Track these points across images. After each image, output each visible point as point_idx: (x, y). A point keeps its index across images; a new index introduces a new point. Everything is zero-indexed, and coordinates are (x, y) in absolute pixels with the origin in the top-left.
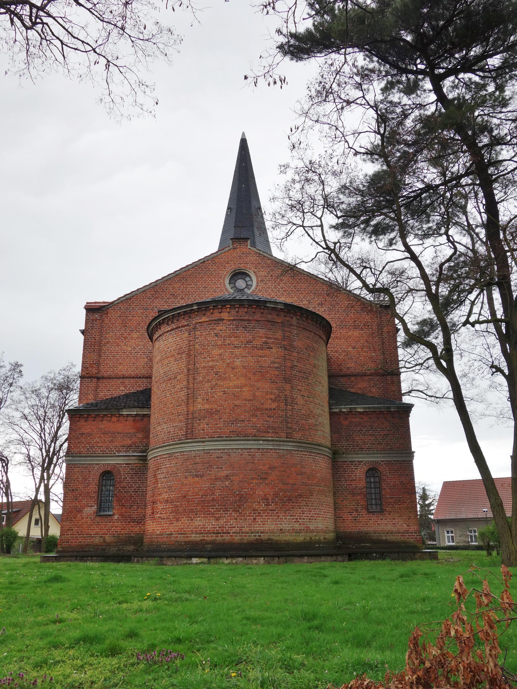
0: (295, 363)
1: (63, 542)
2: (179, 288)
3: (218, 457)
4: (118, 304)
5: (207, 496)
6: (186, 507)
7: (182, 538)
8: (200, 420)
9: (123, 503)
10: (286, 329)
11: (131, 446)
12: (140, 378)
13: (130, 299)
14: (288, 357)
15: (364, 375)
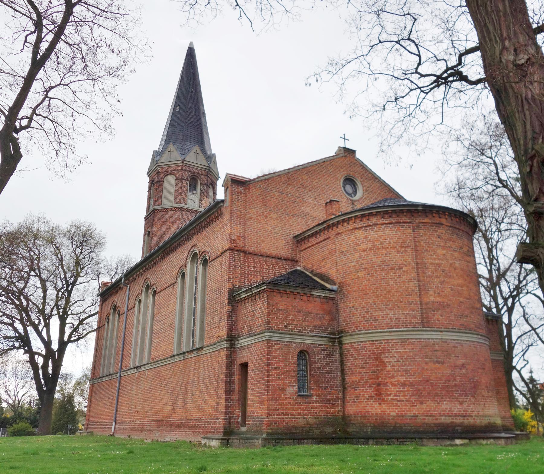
1: (271, 424)
2: (307, 180)
3: (454, 347)
4: (258, 181)
5: (449, 381)
6: (431, 391)
7: (430, 420)
8: (434, 311)
9: (319, 384)
11: (320, 327)
12: (281, 259)
13: (268, 180)
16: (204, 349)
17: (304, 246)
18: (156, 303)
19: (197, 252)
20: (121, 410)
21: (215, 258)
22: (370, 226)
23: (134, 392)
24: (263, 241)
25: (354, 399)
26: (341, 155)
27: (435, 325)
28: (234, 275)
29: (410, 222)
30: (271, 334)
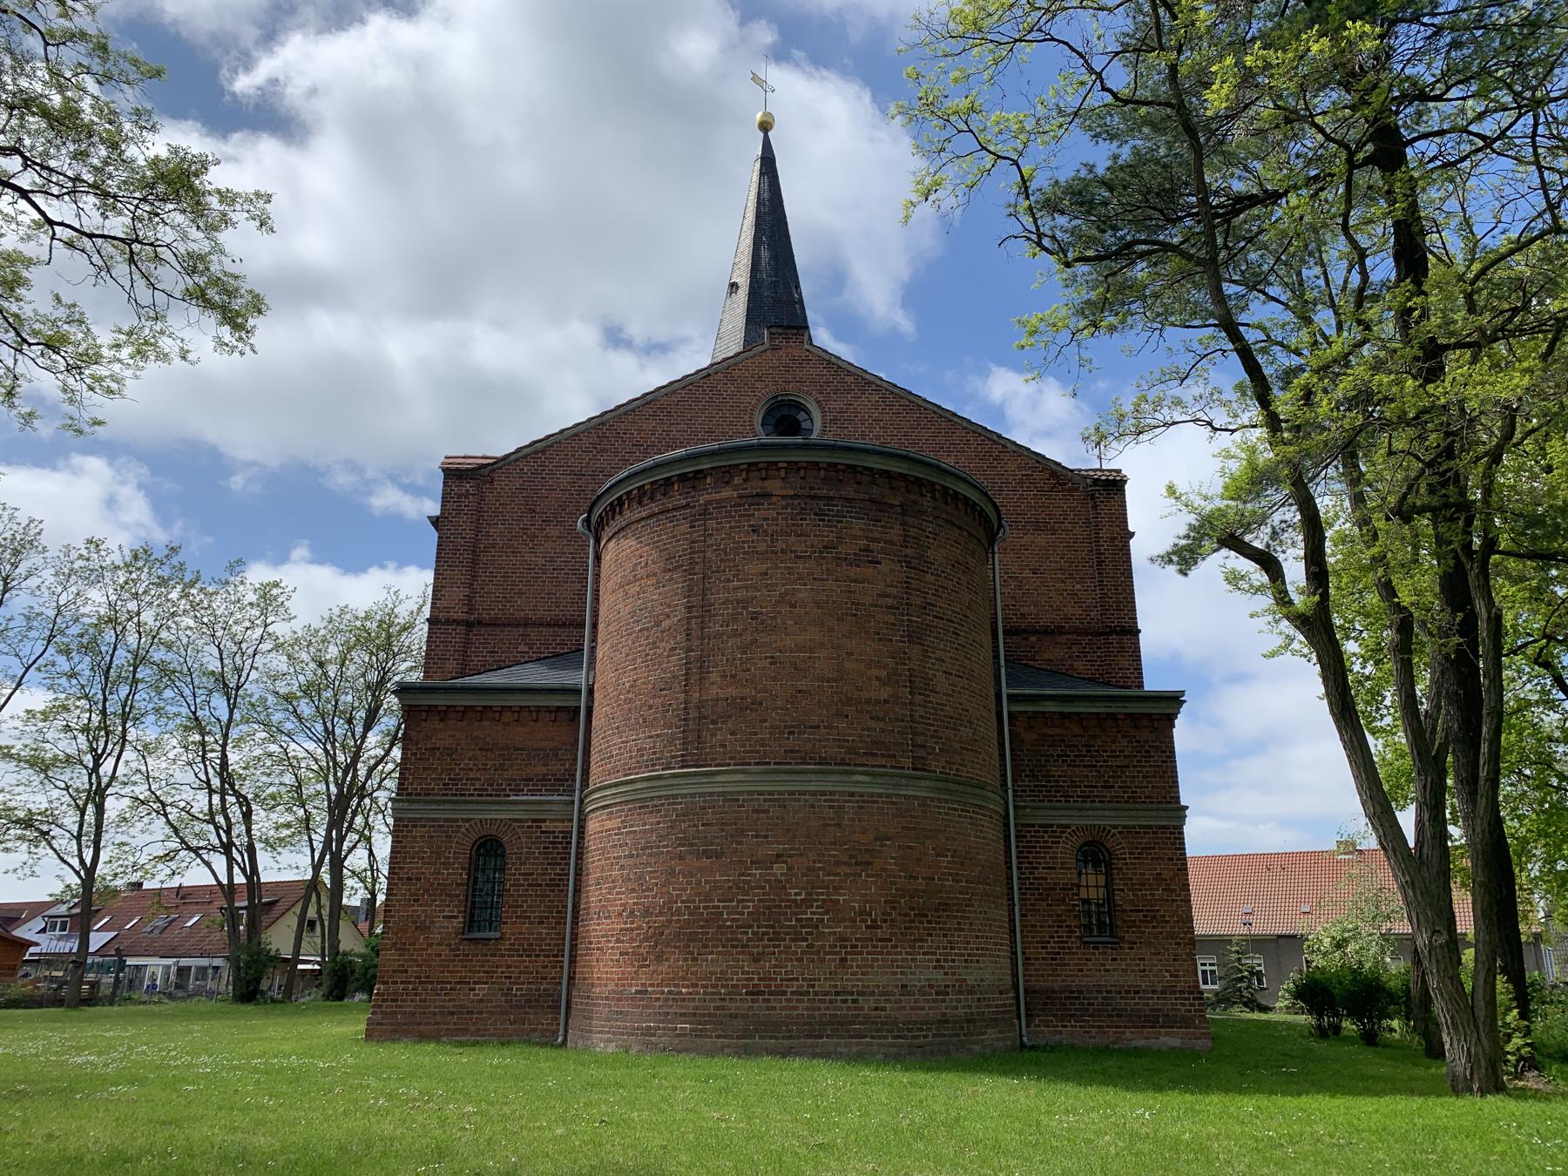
0: (931, 598)
3: (757, 811)
10: (911, 521)
13: (543, 451)
14: (915, 584)
15: (1060, 631)
24: (521, 593)
27: (713, 759)
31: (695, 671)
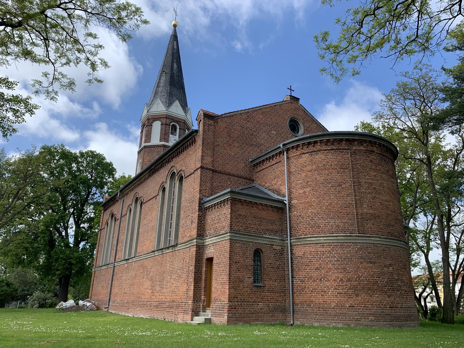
2: (262, 118)
13: (232, 116)
16: (178, 246)
17: (260, 169)
18: (142, 211)
19: (175, 171)
20: (115, 291)
21: (189, 175)
22: (315, 151)
23: (124, 278)
25: (300, 291)
26: (288, 102)
28: (204, 188)
29: (348, 149)
30: (234, 235)
31: (358, 203)
